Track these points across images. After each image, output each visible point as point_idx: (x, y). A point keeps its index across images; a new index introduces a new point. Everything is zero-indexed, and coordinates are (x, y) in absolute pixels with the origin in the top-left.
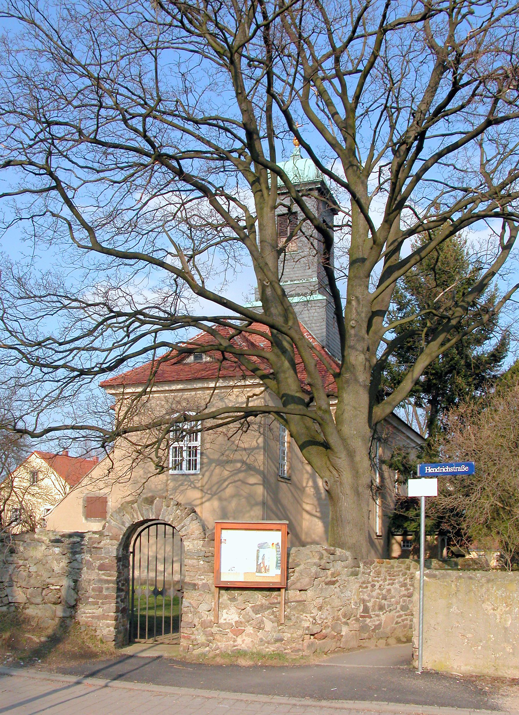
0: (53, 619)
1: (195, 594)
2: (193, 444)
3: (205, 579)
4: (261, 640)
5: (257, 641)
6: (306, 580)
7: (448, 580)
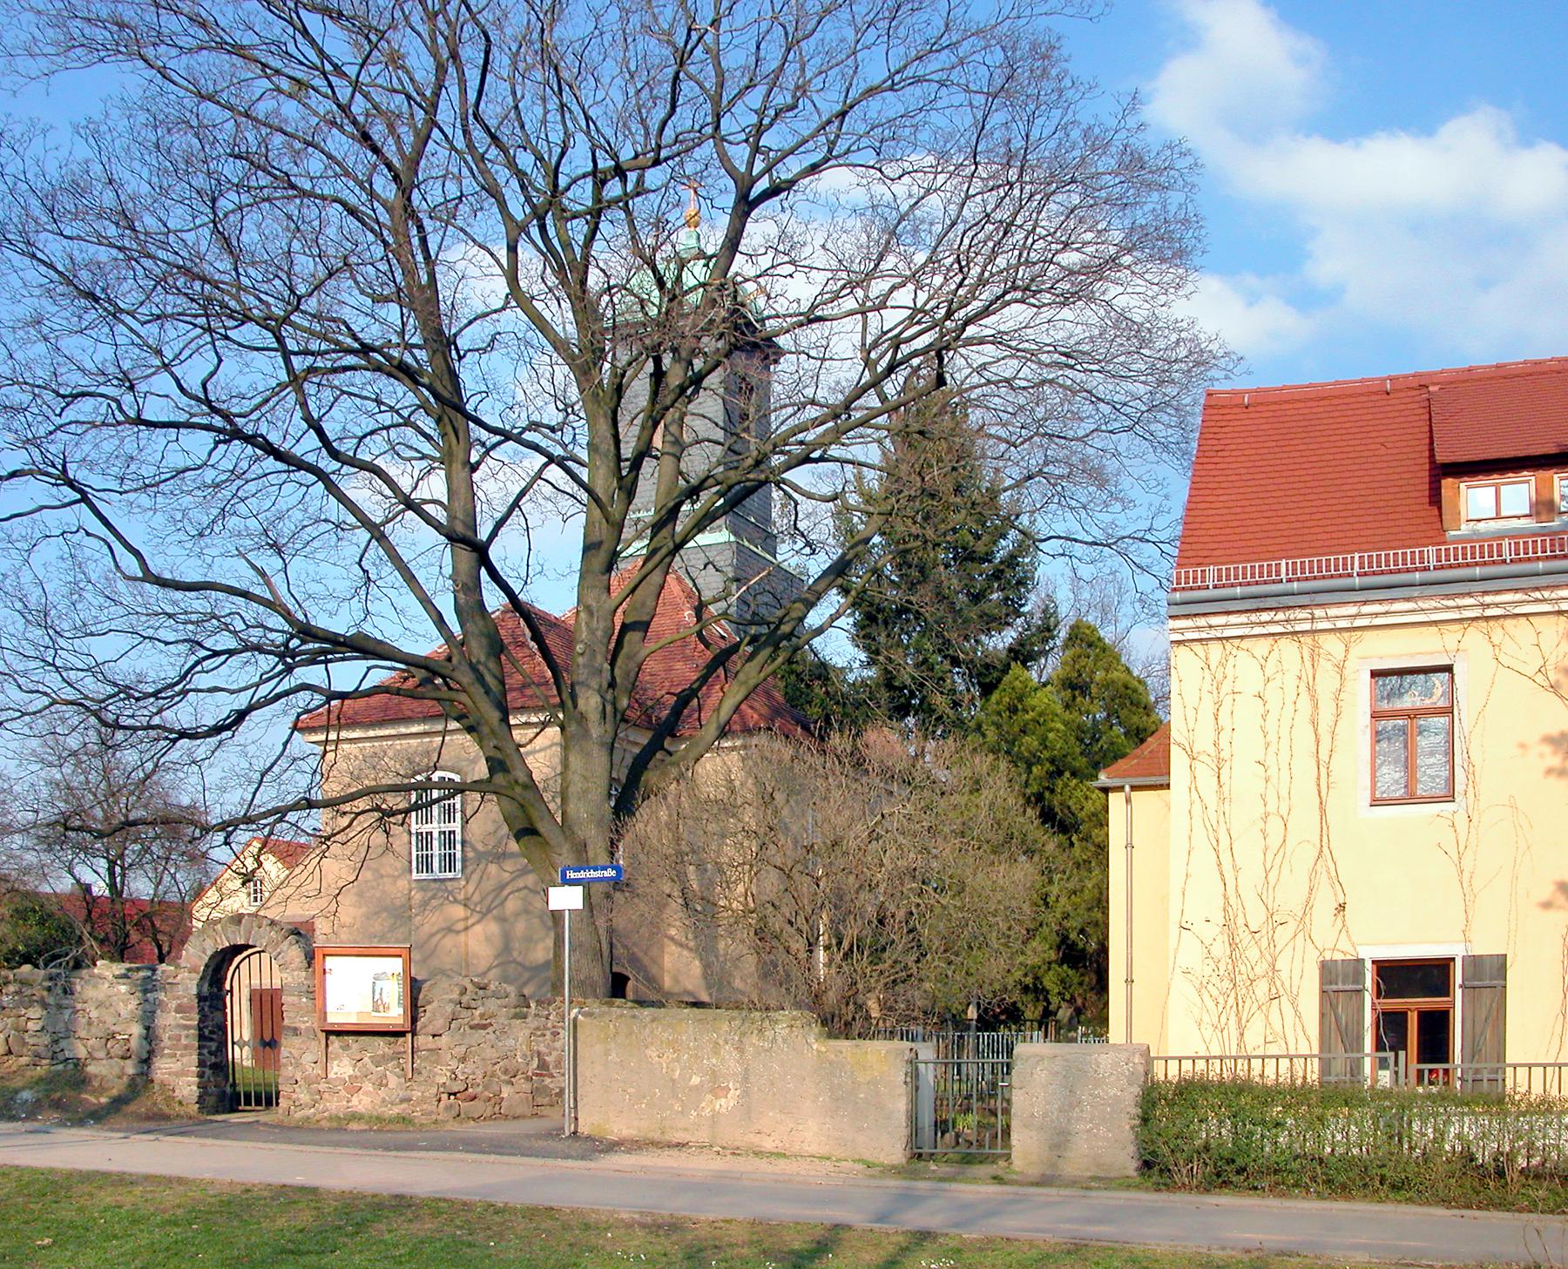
0: (119, 1078)
1: (297, 1041)
2: (425, 828)
3: (306, 1022)
4: (384, 1100)
5: (378, 1101)
6: (439, 1023)
7: (607, 1019)
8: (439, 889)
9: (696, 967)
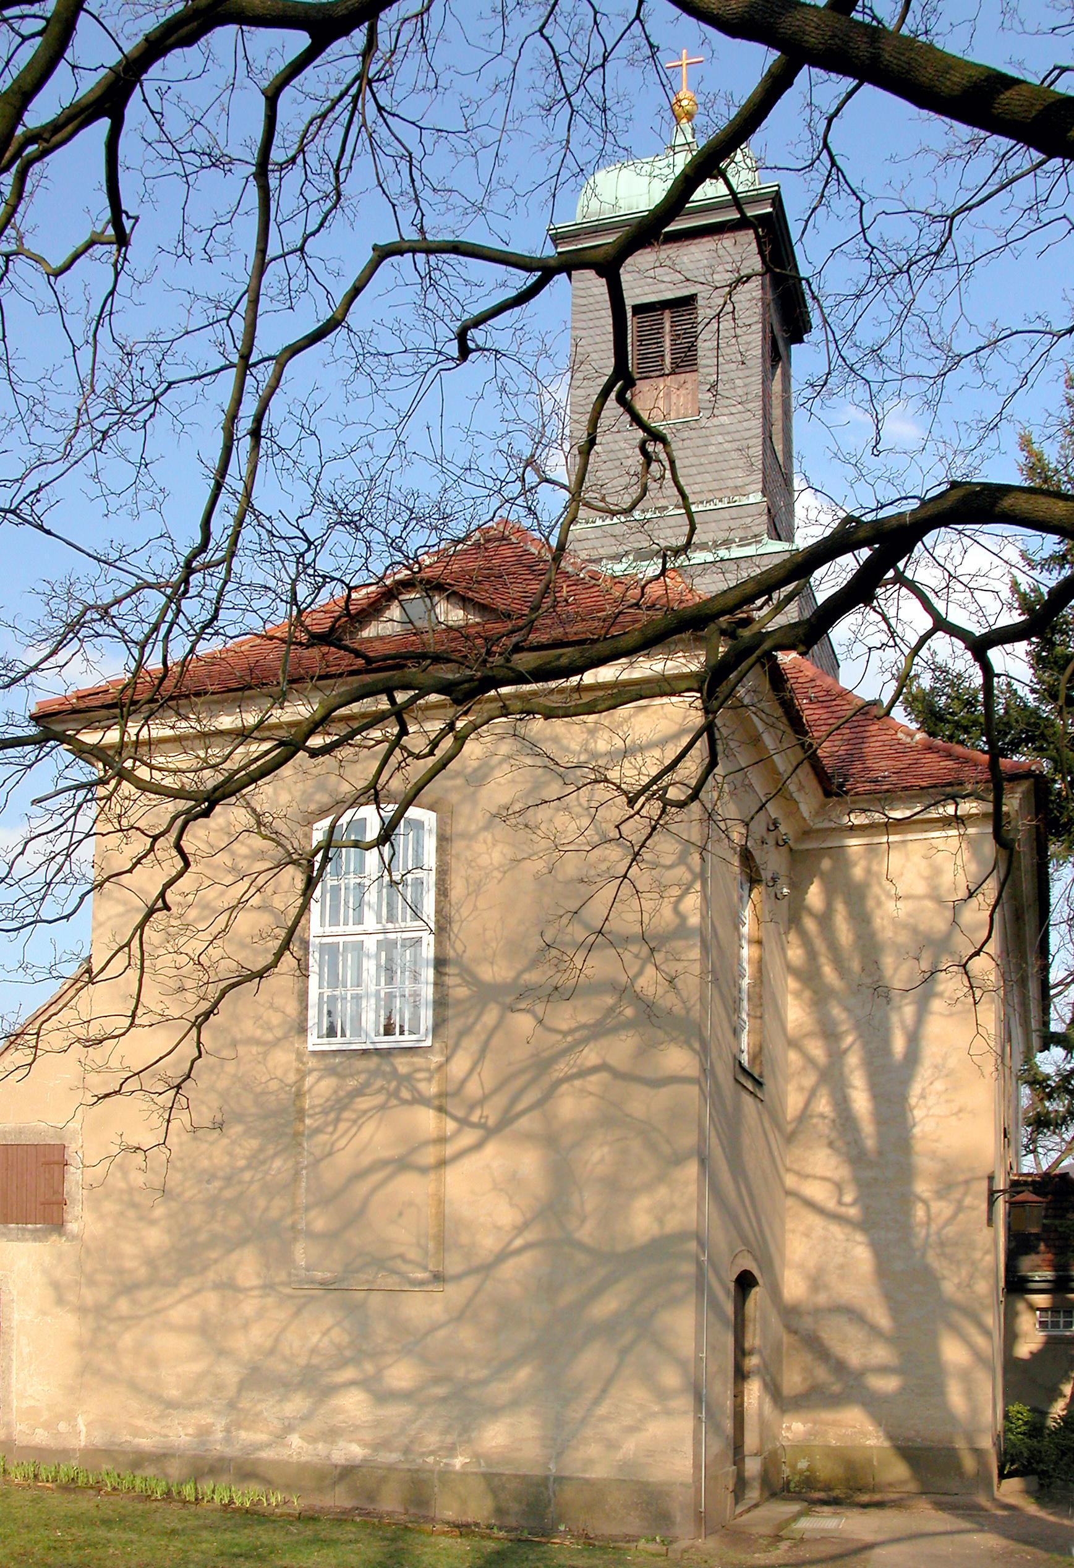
8: (376, 1073)
9: (862, 1254)
